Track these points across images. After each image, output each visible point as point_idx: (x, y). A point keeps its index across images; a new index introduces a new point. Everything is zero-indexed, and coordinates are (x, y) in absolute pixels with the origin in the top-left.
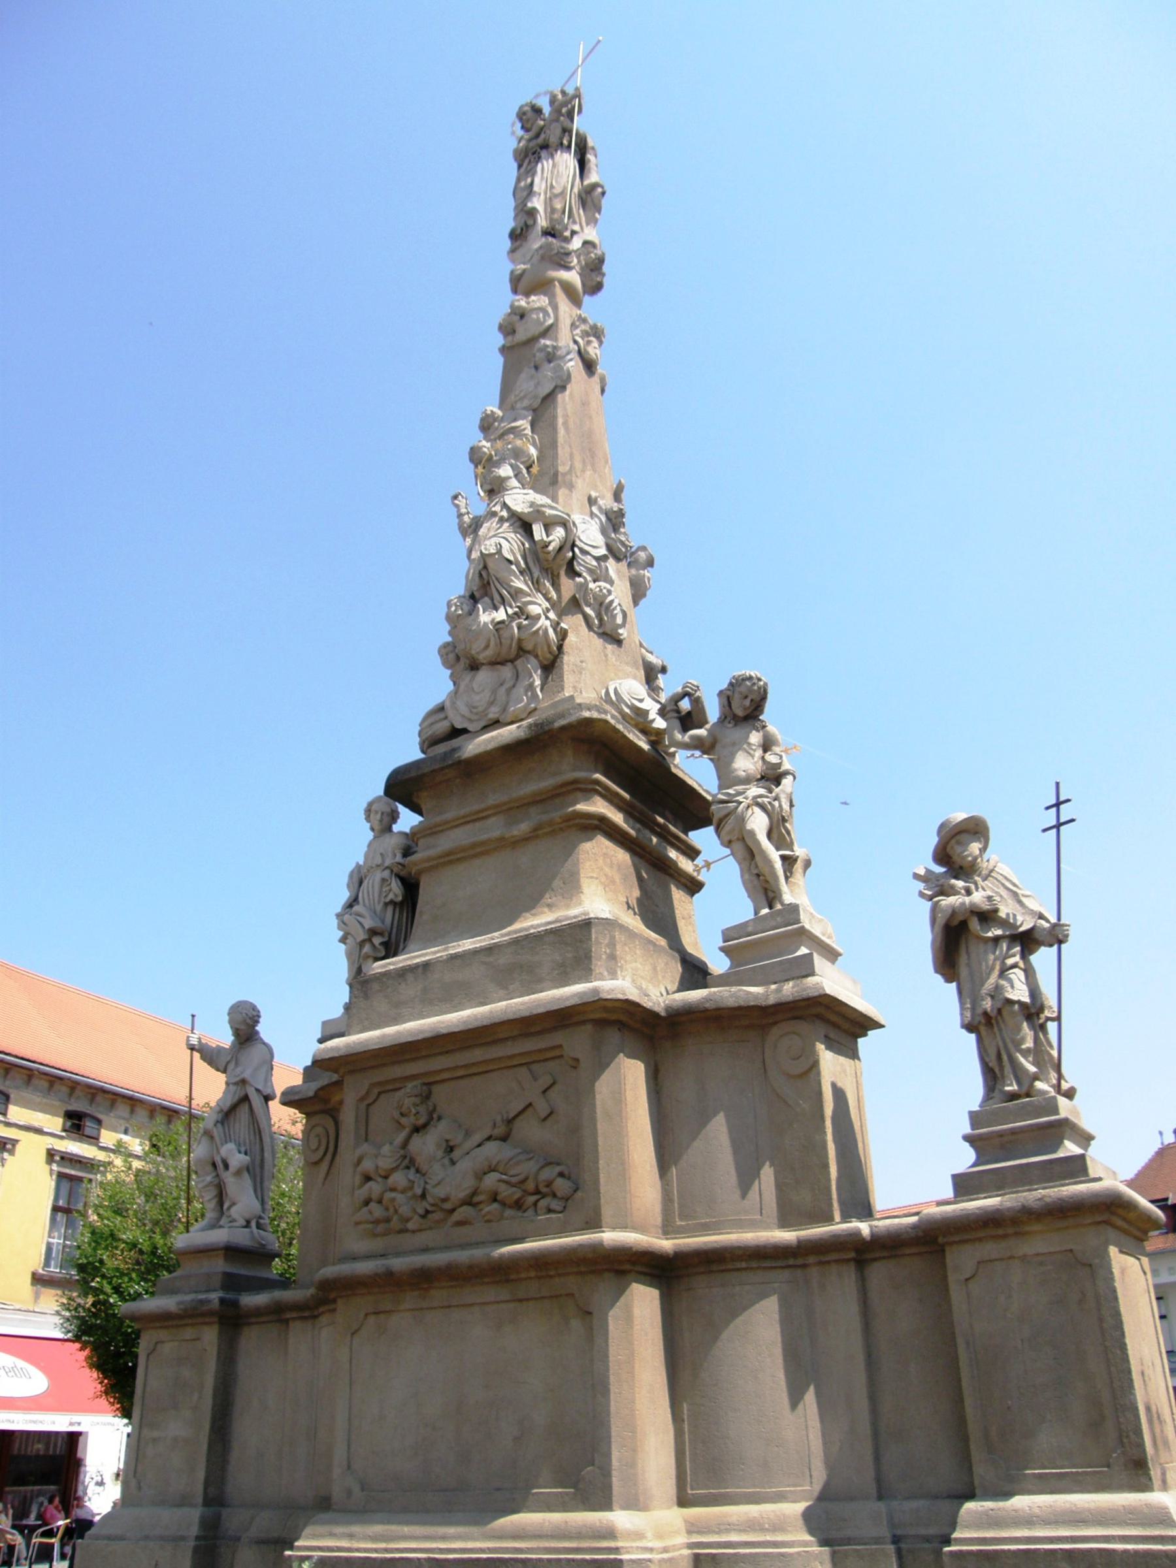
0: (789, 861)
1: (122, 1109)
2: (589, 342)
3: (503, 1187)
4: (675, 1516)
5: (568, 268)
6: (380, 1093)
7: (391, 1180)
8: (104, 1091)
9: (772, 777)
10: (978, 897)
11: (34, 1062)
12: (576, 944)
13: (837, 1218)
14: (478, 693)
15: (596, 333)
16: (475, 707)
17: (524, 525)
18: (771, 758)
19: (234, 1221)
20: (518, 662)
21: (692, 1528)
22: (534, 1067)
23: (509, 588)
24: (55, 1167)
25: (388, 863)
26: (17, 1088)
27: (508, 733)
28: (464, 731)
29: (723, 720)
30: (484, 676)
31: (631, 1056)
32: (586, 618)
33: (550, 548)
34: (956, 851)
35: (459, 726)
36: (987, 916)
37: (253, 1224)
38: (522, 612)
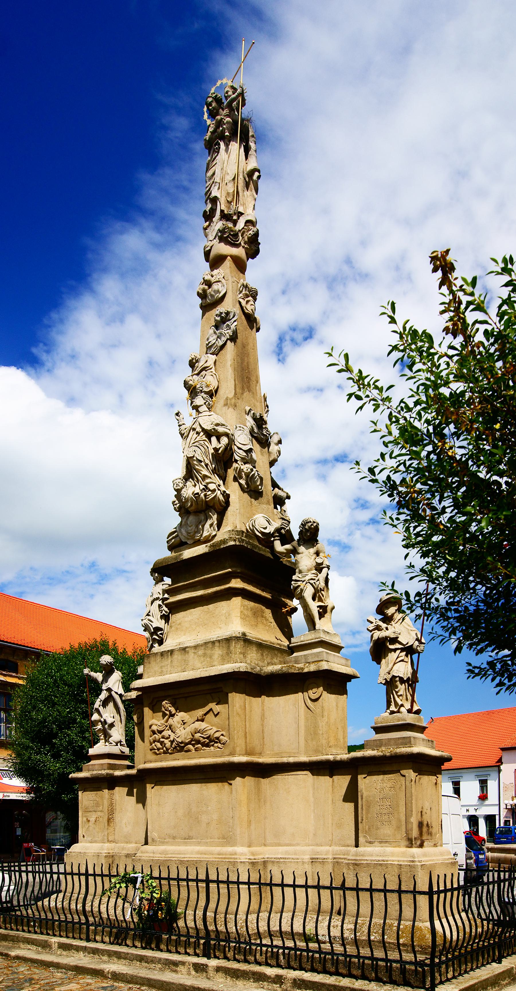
2: (248, 302)
3: (202, 739)
5: (238, 246)
6: (157, 701)
7: (163, 733)
10: (389, 633)
11: (27, 647)
14: (190, 527)
15: (253, 294)
16: (190, 533)
19: (111, 743)
20: (207, 512)
26: (21, 660)
27: (201, 549)
28: (186, 543)
30: (192, 518)
32: (240, 485)
33: (220, 452)
36: (394, 640)
37: (119, 744)
38: (206, 488)
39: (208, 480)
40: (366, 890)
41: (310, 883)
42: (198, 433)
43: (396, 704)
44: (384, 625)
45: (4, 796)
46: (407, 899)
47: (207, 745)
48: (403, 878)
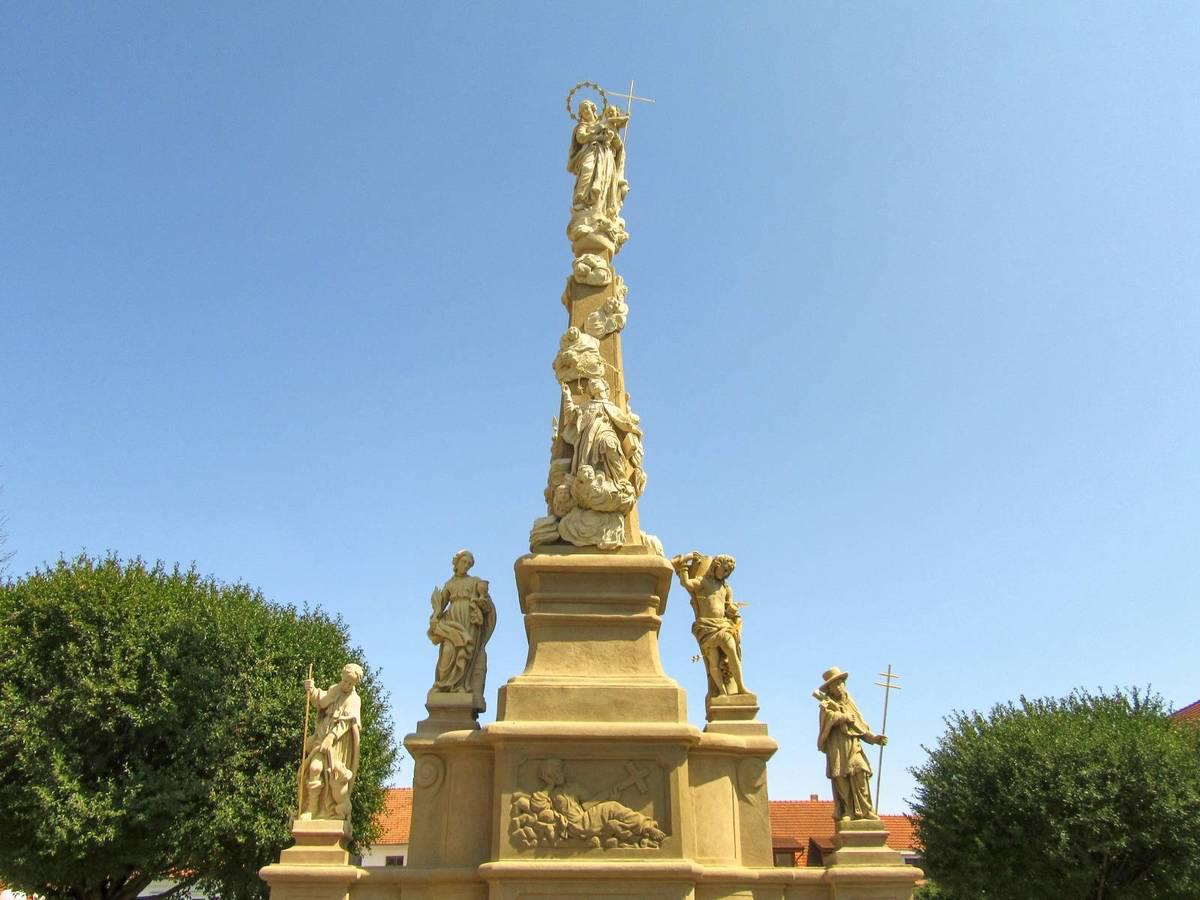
12: (668, 702)
13: (626, 96)
35: (566, 538)
47: (630, 841)
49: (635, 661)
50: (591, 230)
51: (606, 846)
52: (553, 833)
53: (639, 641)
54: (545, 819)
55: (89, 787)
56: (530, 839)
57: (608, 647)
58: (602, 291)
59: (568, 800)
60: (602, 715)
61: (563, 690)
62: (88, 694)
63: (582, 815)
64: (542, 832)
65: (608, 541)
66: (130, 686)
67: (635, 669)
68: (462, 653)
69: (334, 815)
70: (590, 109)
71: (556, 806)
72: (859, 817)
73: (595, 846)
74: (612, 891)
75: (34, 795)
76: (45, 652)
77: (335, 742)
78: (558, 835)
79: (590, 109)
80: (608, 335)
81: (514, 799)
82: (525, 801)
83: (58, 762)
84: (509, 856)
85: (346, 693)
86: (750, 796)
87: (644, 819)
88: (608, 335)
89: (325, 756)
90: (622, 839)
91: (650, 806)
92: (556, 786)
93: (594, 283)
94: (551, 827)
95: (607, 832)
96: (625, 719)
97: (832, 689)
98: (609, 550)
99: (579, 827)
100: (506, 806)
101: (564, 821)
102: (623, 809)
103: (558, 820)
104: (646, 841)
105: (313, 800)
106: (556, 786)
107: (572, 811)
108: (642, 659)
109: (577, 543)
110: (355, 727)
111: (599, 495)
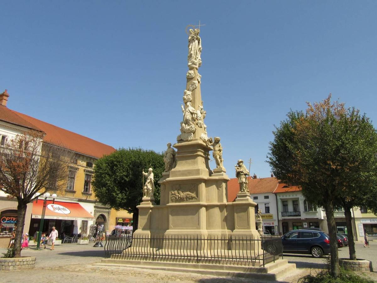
0: (221, 161)
1: (81, 158)
4: (206, 230)
8: (78, 154)
9: (220, 150)
10: (241, 170)
12: (198, 172)
13: (198, 26)
17: (192, 114)
18: (220, 148)
21: (208, 232)
22: (263, 256)
23: (190, 123)
24: (85, 173)
25: (171, 152)
29: (214, 143)
31: (203, 183)
34: (239, 164)
35: (182, 139)
36: (242, 172)
38: (191, 127)
39: (192, 125)
40: (206, 239)
41: (188, 238)
42: (188, 112)
43: (243, 189)
44: (239, 168)
45: (35, 217)
46: (158, 240)
47: (191, 199)
48: (195, 236)
49: (194, 164)
50: (191, 64)
51: (187, 200)
52: (177, 198)
53: (196, 159)
54: (176, 196)
55: (121, 192)
56: (174, 200)
57: (190, 161)
58: (192, 79)
59: (180, 192)
60: (186, 175)
61: (179, 171)
62: (118, 176)
63: (182, 195)
64: (176, 198)
65: (190, 139)
66: (125, 173)
67: (194, 165)
68: (168, 164)
69: (149, 196)
70: (191, 31)
71: (178, 193)
72: (242, 192)
73: (185, 200)
74: (267, 211)
75: (112, 194)
76: (112, 168)
77: (148, 183)
78: (178, 198)
79: (191, 31)
80: (193, 90)
81: (171, 192)
82: (173, 193)
83: (116, 189)
84: (171, 203)
85: (150, 173)
86: (220, 189)
87: (193, 195)
88: (193, 90)
89: (147, 186)
90: (189, 199)
91: (195, 192)
92: (179, 189)
93: (191, 78)
94: (177, 197)
95: (187, 198)
96: (190, 176)
97: (239, 164)
98: (190, 141)
99: (182, 197)
100: (170, 194)
101: (179, 196)
102: (190, 193)
103: (178, 196)
104: (194, 199)
105: (146, 194)
106: (179, 189)
107: (181, 194)
108: (196, 163)
109: (184, 140)
110: (152, 180)
111: (186, 130)
